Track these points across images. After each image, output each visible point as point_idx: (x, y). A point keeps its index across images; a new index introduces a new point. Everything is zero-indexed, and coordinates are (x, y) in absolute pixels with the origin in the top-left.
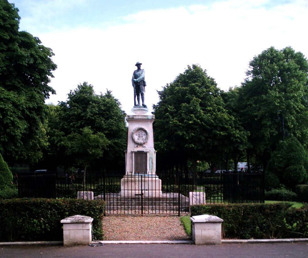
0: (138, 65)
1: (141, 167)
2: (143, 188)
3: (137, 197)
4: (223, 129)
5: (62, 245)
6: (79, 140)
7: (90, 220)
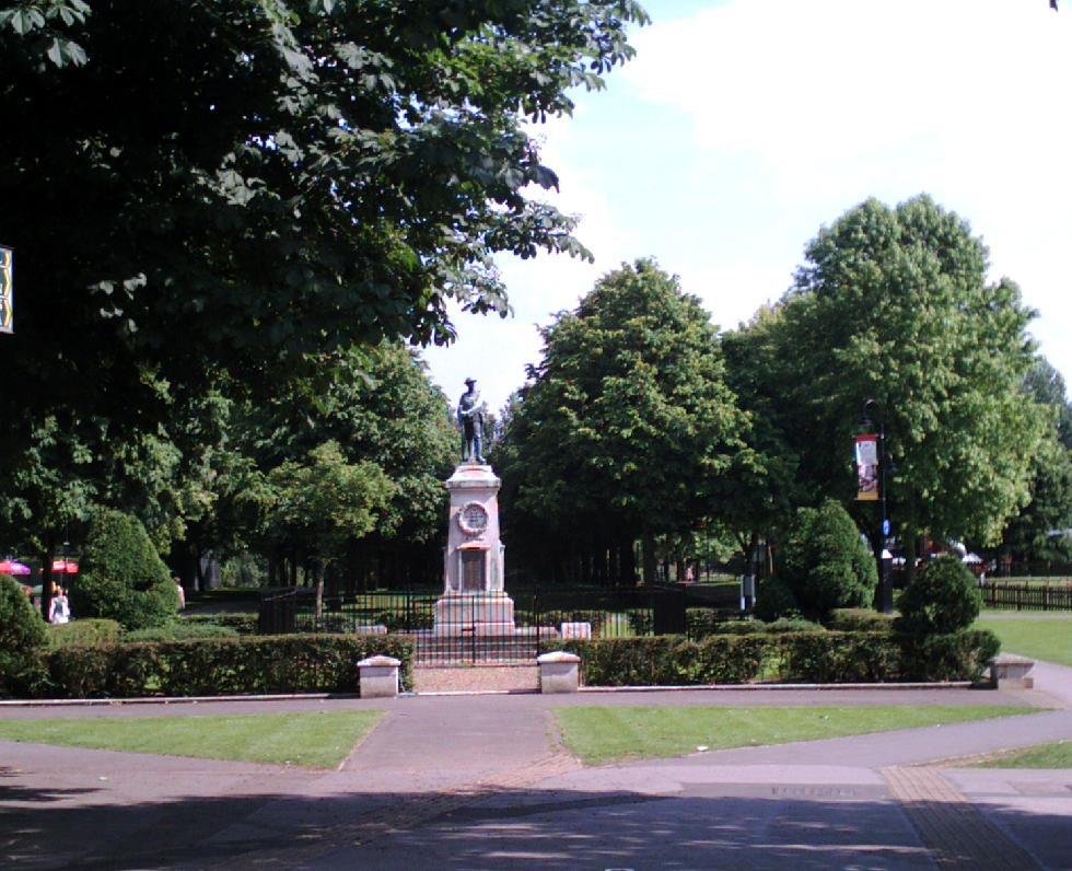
0: (470, 383)
1: (476, 580)
2: (475, 619)
3: (465, 633)
4: (721, 448)
5: (359, 697)
6: (306, 485)
7: (397, 662)
